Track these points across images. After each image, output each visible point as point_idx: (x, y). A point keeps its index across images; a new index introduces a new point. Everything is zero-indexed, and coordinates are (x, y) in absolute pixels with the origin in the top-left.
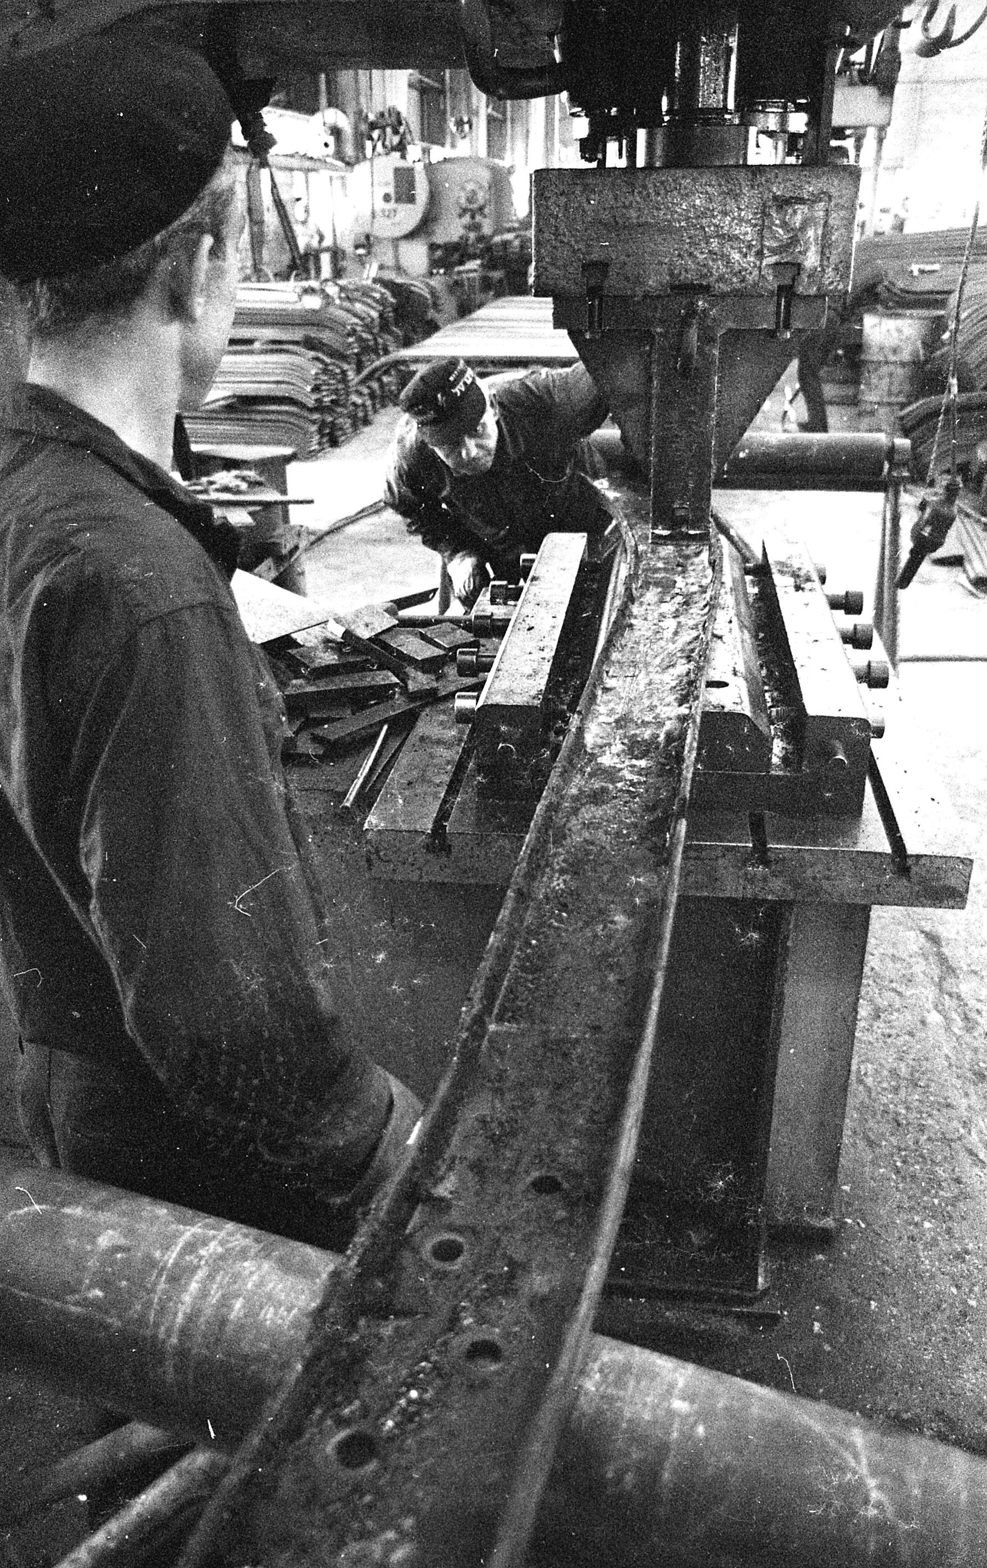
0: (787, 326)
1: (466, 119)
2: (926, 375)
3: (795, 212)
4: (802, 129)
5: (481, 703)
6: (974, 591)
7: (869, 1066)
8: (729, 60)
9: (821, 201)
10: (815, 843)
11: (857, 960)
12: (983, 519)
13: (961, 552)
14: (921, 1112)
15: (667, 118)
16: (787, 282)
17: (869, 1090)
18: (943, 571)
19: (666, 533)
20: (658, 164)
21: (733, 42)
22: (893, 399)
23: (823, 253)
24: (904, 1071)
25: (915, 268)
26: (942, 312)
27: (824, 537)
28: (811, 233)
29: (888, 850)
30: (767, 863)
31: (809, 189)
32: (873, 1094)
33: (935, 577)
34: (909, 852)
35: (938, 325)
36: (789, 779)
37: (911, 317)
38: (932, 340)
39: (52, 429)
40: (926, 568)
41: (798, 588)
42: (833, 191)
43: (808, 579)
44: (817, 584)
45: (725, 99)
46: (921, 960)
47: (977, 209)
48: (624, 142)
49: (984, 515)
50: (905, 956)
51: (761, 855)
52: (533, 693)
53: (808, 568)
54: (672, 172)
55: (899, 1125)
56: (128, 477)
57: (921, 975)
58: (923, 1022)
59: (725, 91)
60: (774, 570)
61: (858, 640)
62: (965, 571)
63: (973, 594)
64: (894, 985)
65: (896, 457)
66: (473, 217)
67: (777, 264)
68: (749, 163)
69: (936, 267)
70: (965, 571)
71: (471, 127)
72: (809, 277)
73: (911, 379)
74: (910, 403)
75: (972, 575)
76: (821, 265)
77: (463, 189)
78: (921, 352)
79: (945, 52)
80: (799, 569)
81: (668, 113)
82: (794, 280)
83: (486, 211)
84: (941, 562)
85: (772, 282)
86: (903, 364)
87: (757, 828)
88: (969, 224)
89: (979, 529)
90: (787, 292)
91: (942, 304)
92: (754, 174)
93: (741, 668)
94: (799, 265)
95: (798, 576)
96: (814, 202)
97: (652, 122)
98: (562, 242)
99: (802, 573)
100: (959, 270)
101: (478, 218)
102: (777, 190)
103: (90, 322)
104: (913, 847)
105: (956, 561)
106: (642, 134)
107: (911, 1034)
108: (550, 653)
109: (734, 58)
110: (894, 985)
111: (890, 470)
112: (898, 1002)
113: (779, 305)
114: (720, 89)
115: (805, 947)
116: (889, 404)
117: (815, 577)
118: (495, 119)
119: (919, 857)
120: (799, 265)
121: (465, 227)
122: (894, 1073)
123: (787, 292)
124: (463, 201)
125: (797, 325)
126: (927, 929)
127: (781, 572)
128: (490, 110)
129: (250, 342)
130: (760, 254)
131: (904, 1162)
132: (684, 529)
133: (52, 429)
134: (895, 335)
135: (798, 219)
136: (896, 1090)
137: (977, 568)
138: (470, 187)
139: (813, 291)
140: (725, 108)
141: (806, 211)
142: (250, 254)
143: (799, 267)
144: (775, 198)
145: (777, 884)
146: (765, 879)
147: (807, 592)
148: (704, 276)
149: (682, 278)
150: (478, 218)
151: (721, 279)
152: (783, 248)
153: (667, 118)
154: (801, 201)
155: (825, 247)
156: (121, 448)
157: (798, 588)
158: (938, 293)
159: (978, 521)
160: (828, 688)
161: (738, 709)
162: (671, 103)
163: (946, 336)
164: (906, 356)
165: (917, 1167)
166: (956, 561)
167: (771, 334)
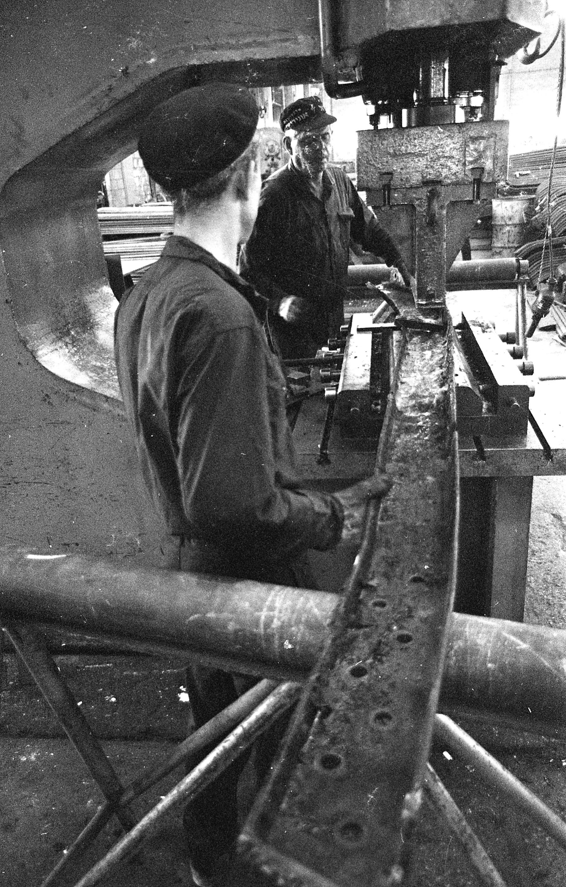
0: (478, 198)
1: (263, 108)
2: (530, 230)
3: (480, 143)
4: (479, 105)
5: (340, 390)
6: (562, 342)
7: (532, 578)
8: (444, 75)
9: (492, 137)
10: (506, 447)
11: (526, 510)
12: (565, 306)
13: (555, 323)
14: (560, 598)
15: (416, 103)
16: (477, 177)
17: (533, 590)
18: (545, 333)
19: (424, 303)
20: (413, 125)
21: (446, 66)
22: (511, 245)
23: (494, 162)
24: (549, 579)
25: (517, 173)
26: (534, 196)
27: (488, 311)
28: (488, 153)
29: (542, 448)
30: (484, 458)
31: (486, 133)
32: (536, 591)
33: (541, 337)
34: (552, 448)
35: (532, 202)
36: (496, 412)
37: (517, 199)
38: (530, 212)
39: (185, 254)
40: (537, 333)
41: (484, 331)
42: (497, 132)
43: (488, 327)
44: (493, 329)
45: (444, 92)
46: (553, 526)
47: (556, 139)
48: (391, 115)
49: (564, 303)
50: (545, 525)
51: (481, 455)
52: (365, 384)
53: (486, 321)
54: (422, 128)
55: (550, 605)
56: (217, 273)
57: (554, 534)
58: (557, 556)
59: (444, 89)
60: (470, 324)
61: (516, 355)
62: (557, 333)
63: (562, 344)
64: (541, 539)
65: (522, 269)
66: (273, 160)
67: (473, 169)
68: (456, 122)
69: (529, 172)
70: (557, 333)
71: (266, 112)
72: (488, 173)
73: (520, 233)
74: (520, 247)
75: (561, 335)
76: (494, 168)
77: (267, 145)
78: (525, 218)
79: (537, 61)
80: (483, 323)
81: (416, 101)
82: (481, 175)
83: (280, 156)
84: (544, 329)
85: (471, 179)
86: (515, 225)
87: (478, 443)
88: (552, 146)
89: (563, 311)
90: (478, 182)
91: (535, 191)
92: (460, 127)
93: (463, 368)
94: (483, 168)
95: (483, 326)
96: (489, 138)
97: (409, 104)
98: (370, 164)
99: (485, 325)
100: (549, 171)
101: (276, 160)
102: (472, 134)
103: (202, 205)
104: (553, 446)
105: (552, 328)
106: (405, 112)
107: (552, 562)
108: (368, 367)
109: (447, 73)
110: (541, 539)
111: (518, 277)
112: (543, 547)
113: (474, 187)
114: (440, 87)
115: (503, 502)
116: (509, 248)
117: (491, 326)
118: (277, 106)
119: (556, 450)
120: (483, 168)
121: (268, 165)
122: (545, 581)
123: (478, 182)
124: (267, 152)
125: (483, 197)
126: (554, 513)
127: (474, 325)
128: (274, 102)
129: (158, 234)
130: (464, 164)
131: (554, 622)
132: (433, 301)
133: (185, 253)
134: (510, 209)
135: (481, 147)
136: (547, 589)
137: (564, 331)
138: (270, 144)
139: (490, 180)
140: (444, 98)
141: (485, 142)
142: (149, 187)
143: (483, 169)
144: (471, 138)
145: (489, 469)
146: (483, 467)
147: (488, 333)
148: (438, 176)
149: (428, 177)
150: (276, 160)
151: (446, 177)
152: (475, 161)
153: (416, 103)
154: (483, 138)
155: (495, 158)
156: (214, 260)
157: (484, 331)
158: (532, 186)
159: (562, 307)
160: (506, 373)
161: (465, 385)
162: (418, 97)
163: (538, 208)
164: (516, 221)
165: (561, 624)
166: (552, 328)
167: (470, 202)
